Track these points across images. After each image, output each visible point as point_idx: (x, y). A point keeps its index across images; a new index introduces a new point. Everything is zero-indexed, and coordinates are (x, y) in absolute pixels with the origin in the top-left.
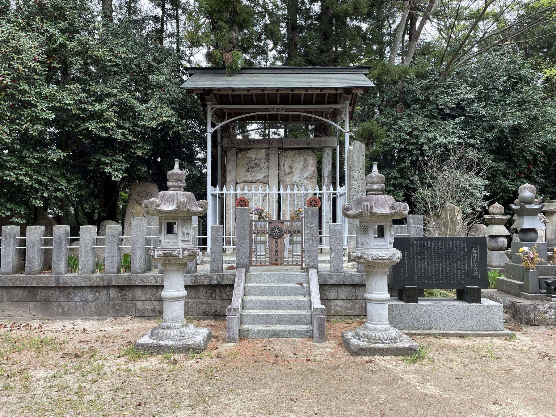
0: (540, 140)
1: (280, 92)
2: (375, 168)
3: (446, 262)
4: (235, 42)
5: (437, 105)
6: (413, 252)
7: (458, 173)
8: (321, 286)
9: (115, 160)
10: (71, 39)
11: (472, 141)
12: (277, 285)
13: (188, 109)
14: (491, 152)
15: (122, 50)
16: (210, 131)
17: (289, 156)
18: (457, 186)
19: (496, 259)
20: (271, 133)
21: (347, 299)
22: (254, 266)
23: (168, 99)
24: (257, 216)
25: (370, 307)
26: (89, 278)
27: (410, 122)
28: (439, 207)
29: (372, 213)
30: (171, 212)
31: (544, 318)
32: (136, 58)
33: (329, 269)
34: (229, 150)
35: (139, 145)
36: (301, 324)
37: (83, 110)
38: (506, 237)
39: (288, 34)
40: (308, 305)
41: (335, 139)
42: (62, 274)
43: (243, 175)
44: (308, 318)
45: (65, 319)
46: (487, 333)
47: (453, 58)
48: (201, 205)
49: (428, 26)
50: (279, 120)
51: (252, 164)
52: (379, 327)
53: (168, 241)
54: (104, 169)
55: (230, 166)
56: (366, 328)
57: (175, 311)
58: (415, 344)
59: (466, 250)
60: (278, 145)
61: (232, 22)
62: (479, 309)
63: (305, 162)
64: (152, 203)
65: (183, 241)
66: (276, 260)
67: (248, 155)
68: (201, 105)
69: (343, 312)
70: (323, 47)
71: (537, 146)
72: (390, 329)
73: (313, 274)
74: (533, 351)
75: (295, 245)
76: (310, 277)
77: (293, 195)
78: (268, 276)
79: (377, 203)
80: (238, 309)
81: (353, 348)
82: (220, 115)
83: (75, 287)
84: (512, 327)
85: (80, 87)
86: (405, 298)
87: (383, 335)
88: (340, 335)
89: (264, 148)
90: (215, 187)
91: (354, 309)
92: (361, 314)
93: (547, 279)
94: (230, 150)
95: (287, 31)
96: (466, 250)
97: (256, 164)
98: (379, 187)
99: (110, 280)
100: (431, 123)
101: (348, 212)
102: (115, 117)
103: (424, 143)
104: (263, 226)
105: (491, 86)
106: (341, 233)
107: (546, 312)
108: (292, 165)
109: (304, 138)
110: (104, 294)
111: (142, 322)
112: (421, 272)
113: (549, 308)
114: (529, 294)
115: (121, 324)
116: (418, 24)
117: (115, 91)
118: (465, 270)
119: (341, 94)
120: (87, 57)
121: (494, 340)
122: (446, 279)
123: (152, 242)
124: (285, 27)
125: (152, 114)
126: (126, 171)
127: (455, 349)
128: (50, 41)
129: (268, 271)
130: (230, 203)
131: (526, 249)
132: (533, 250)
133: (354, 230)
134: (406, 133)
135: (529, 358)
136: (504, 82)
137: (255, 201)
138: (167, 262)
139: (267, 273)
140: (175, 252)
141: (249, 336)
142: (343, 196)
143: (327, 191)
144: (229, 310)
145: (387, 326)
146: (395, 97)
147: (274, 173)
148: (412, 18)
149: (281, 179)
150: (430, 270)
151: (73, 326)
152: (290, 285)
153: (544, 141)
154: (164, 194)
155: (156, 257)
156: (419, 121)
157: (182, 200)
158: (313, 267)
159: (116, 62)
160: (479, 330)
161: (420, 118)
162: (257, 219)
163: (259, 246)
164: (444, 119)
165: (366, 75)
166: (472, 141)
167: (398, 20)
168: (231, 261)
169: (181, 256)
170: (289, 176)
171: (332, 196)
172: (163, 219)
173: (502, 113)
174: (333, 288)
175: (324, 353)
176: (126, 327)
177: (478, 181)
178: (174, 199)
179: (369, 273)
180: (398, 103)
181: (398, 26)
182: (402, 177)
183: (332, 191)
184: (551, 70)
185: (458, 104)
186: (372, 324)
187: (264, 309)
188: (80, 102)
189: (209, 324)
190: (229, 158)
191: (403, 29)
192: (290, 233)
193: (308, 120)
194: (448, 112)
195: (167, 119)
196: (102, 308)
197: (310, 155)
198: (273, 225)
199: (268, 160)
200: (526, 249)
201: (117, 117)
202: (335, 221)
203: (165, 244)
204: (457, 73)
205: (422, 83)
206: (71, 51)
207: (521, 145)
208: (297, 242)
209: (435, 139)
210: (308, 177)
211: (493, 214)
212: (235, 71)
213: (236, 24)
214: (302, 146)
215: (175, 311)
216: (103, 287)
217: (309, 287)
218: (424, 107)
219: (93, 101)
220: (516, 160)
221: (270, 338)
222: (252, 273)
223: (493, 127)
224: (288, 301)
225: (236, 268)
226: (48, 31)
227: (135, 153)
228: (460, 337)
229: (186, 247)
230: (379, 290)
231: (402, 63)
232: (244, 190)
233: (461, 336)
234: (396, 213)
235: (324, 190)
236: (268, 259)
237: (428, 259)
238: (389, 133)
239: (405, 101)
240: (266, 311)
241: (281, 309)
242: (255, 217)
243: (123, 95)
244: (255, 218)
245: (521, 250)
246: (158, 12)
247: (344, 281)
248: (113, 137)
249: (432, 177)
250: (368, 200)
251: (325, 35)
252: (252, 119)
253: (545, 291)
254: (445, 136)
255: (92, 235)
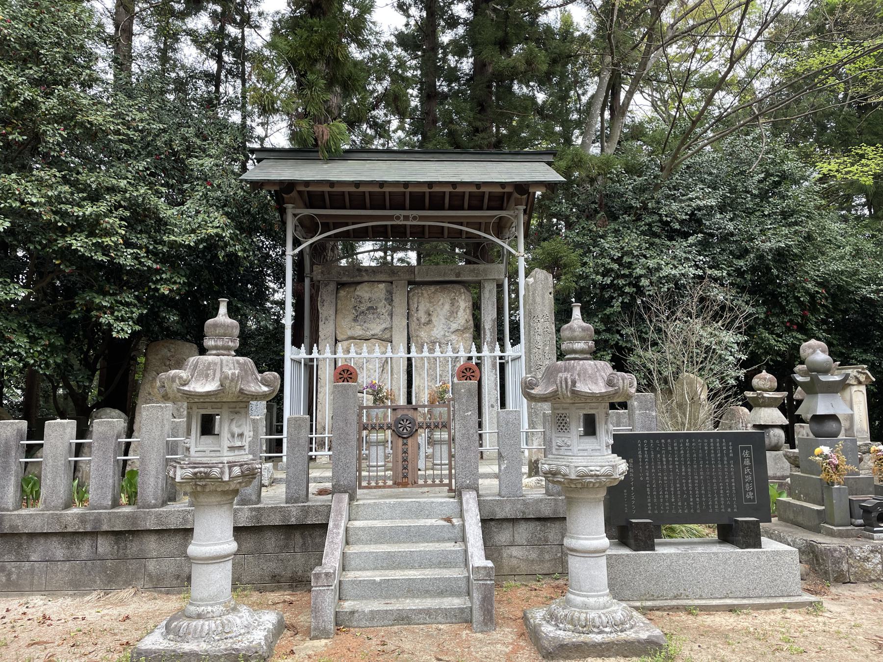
0: (819, 271)
1: (409, 190)
2: (577, 312)
3: (699, 476)
4: (336, 112)
5: (660, 215)
6: (643, 458)
7: (697, 324)
8: (485, 522)
9: (121, 303)
10: (48, 95)
11: (716, 273)
12: (407, 523)
13: (253, 216)
14: (742, 289)
15: (139, 116)
16: (292, 253)
17: (425, 295)
18: (698, 344)
19: (777, 464)
20: (395, 261)
21: (530, 544)
22: (365, 488)
23: (218, 199)
24: (371, 397)
25: (575, 564)
26: (59, 518)
27: (618, 241)
28: (671, 379)
29: (574, 393)
30: (208, 394)
31: (864, 570)
32: (164, 131)
33: (497, 490)
34: (324, 283)
35: (164, 276)
36: (451, 595)
37: (64, 215)
38: (781, 427)
39: (421, 105)
40: (462, 558)
41: (502, 267)
42: (8, 510)
43: (348, 327)
44: (463, 585)
45: (11, 596)
46: (774, 601)
47: (682, 143)
48: (266, 381)
49: (637, 97)
50: (408, 235)
51: (363, 308)
52: (592, 601)
53: (201, 449)
54: (99, 317)
55: (326, 311)
56: (568, 602)
57: (213, 582)
58: (657, 632)
59: (731, 455)
60: (408, 277)
61: (331, 79)
62: (758, 558)
63: (452, 304)
64: (173, 379)
65: (231, 448)
66: (405, 477)
67: (357, 293)
68: (276, 209)
69: (524, 568)
70: (479, 124)
71: (814, 280)
72: (611, 605)
73: (470, 500)
74: (858, 634)
75: (438, 447)
76: (465, 506)
77: (432, 360)
78: (389, 505)
79: (583, 373)
80: (334, 573)
81: (546, 643)
82: (308, 227)
83: (32, 535)
84: (812, 588)
85: (58, 174)
86: (632, 541)
87: (600, 617)
88: (520, 614)
89: (384, 282)
90: (299, 347)
91: (542, 561)
92: (556, 571)
93: (864, 501)
94: (326, 285)
95: (420, 101)
96: (731, 455)
97: (369, 309)
98: (586, 347)
99: (98, 520)
100: (651, 244)
101: (533, 391)
102: (120, 227)
103: (641, 276)
104: (380, 415)
105: (740, 187)
106: (518, 425)
107: (867, 559)
108: (431, 309)
109: (451, 267)
110: (85, 548)
111: (155, 599)
112: (658, 495)
113: (872, 551)
114: (835, 528)
115: (116, 605)
116: (623, 95)
117: (123, 183)
118: (731, 490)
119: (510, 195)
120: (75, 126)
121: (788, 615)
122: (701, 506)
123: (180, 450)
124: (417, 96)
125: (189, 223)
126: (139, 321)
127: (727, 637)
128: (8, 95)
129: (391, 497)
130: (326, 374)
131: (826, 450)
132: (837, 452)
133: (539, 420)
134: (612, 259)
135: (856, 650)
136: (760, 182)
137: (368, 370)
138: (199, 489)
139: (387, 501)
140: (214, 469)
141: (355, 624)
142: (517, 361)
143: (489, 353)
144: (318, 576)
145: (606, 599)
146: (592, 203)
147: (400, 323)
148: (613, 88)
149: (412, 333)
150: (671, 492)
151: (24, 609)
152: (429, 522)
153: (825, 274)
154: (197, 362)
155: (178, 479)
156: (633, 240)
157: (230, 372)
158: (468, 488)
159: (127, 135)
160: (760, 597)
161: (634, 236)
162: (371, 404)
163: (373, 449)
164: (671, 239)
165: (549, 164)
166: (716, 273)
167: (592, 89)
168: (324, 478)
169: (226, 478)
170: (427, 328)
171: (498, 361)
172: (194, 408)
173: (758, 229)
174: (505, 525)
175: (493, 656)
176: (124, 611)
177: (729, 337)
178: (215, 371)
179: (570, 501)
180: (598, 213)
181: (593, 97)
182: (608, 330)
183: (498, 353)
184: (829, 164)
185: (693, 214)
186: (578, 595)
187: (383, 568)
188: (59, 199)
189: (282, 598)
190: (324, 297)
191: (602, 99)
192: (428, 427)
193: (455, 236)
194: (677, 226)
195: (215, 231)
196: (82, 572)
197: (460, 294)
198: (400, 414)
199: (390, 300)
200: (826, 450)
201: (126, 227)
202: (503, 405)
203: (197, 454)
204: (688, 167)
205: (635, 181)
206: (46, 115)
207: (790, 279)
208: (441, 442)
209: (659, 269)
210: (457, 330)
211: (759, 390)
212: (335, 155)
213: (338, 82)
214: (447, 279)
215: (213, 582)
216: (85, 534)
217: (464, 525)
218: (639, 218)
219: (84, 199)
220: (784, 303)
221: (393, 625)
222: (361, 502)
223: (746, 252)
224: (425, 552)
225: (332, 493)
226: (6, 79)
227: (157, 290)
228: (731, 611)
229: (237, 459)
230: (590, 531)
231: (602, 150)
232: (349, 352)
233: (731, 609)
234: (616, 393)
235: (486, 352)
236: (389, 473)
237: (668, 470)
238: (585, 259)
239: (609, 209)
240: (387, 572)
241: (413, 568)
242: (367, 399)
243: (137, 191)
244: (368, 400)
245: (817, 451)
246: (212, 66)
247: (524, 513)
248: (117, 261)
249: (659, 330)
250: (566, 370)
251: (481, 106)
252: (363, 235)
253: (861, 521)
254: (674, 265)
255: (67, 436)
